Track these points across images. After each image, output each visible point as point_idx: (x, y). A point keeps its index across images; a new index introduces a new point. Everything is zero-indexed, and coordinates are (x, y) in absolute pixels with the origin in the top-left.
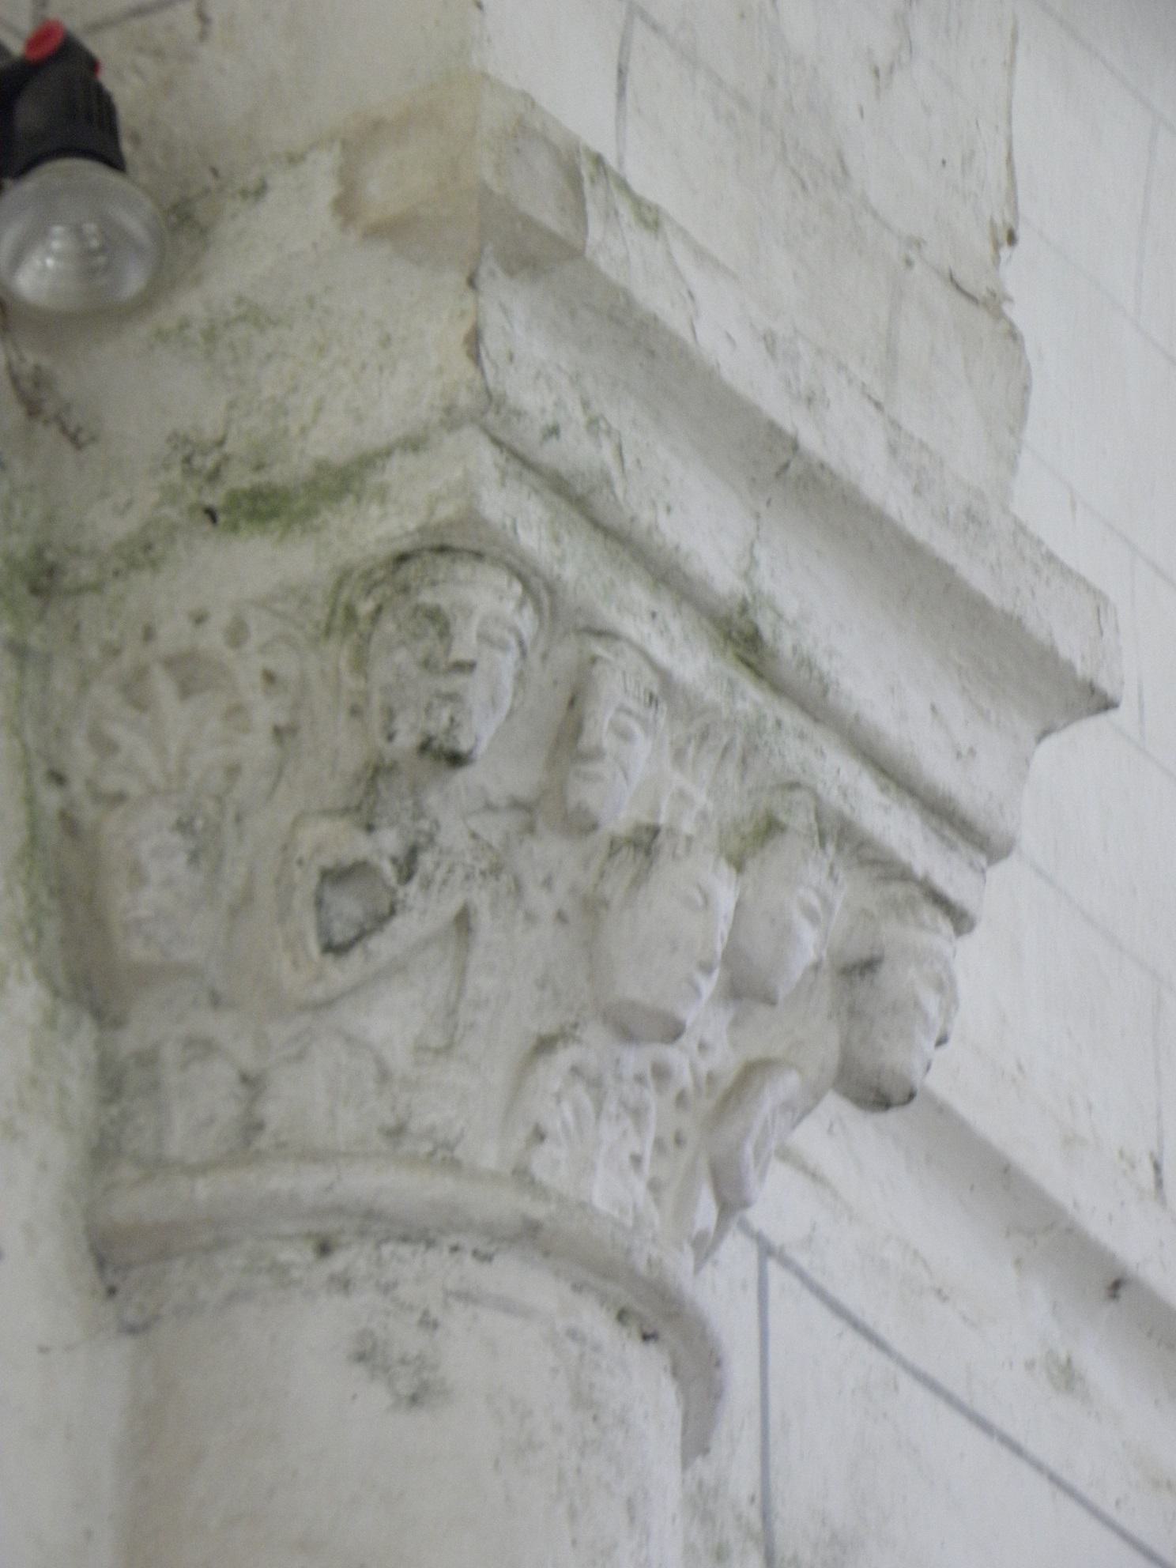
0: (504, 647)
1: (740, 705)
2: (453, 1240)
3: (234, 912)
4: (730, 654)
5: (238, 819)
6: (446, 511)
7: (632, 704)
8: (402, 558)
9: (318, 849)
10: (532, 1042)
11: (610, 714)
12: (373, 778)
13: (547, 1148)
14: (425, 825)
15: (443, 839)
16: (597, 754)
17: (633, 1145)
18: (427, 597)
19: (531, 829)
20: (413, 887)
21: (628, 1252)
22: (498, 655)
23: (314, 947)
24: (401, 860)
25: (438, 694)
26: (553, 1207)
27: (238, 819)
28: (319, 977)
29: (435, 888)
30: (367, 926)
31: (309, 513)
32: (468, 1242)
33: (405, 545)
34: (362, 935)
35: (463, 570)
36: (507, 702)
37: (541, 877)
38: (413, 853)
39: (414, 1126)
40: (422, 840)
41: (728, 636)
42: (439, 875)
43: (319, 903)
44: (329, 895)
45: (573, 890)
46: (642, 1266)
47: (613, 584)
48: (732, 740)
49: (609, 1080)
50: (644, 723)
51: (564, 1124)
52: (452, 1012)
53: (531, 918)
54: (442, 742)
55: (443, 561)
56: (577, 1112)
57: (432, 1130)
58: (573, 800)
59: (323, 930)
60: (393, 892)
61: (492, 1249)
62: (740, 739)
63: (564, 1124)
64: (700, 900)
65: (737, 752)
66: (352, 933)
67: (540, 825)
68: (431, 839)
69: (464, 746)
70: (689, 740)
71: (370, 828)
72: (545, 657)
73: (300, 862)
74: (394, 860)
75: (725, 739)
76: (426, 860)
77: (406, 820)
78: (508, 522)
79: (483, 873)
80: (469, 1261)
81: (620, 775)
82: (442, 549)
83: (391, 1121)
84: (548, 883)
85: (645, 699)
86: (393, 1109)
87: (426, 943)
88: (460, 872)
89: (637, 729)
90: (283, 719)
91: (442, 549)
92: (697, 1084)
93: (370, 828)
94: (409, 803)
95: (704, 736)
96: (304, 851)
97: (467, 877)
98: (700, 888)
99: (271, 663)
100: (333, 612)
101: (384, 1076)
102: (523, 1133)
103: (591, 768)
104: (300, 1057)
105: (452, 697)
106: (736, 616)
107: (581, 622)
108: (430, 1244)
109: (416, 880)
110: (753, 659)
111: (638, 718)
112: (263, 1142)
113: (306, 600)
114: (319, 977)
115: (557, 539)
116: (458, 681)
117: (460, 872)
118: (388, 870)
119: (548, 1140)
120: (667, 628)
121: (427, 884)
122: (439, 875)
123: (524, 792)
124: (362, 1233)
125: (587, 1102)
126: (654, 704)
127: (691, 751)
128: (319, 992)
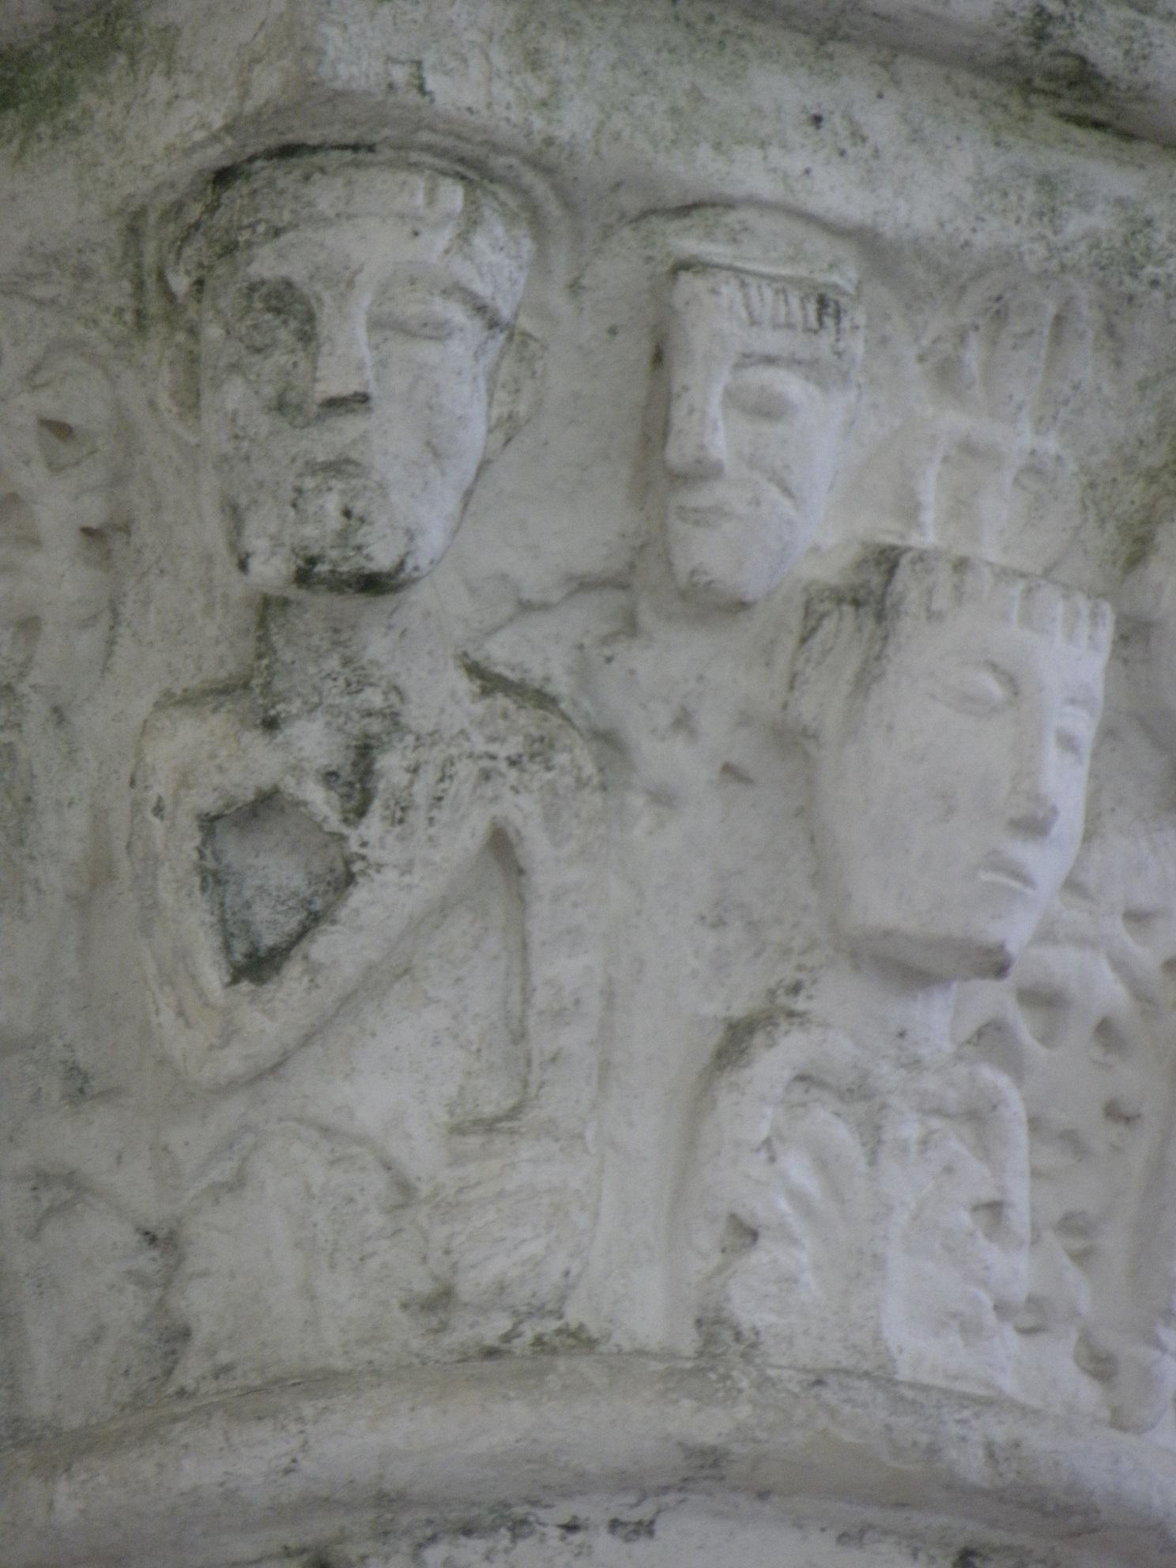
0: (439, 331)
1: (1076, 224)
2: (564, 1511)
3: (82, 904)
4: (1042, 116)
5: (59, 715)
6: (268, 83)
7: (773, 341)
8: (223, 177)
9: (185, 781)
10: (715, 1037)
11: (724, 377)
12: (262, 623)
13: (760, 1257)
14: (374, 698)
15: (416, 716)
16: (703, 472)
17: (977, 1179)
18: (265, 264)
19: (630, 627)
20: (373, 826)
21: (932, 1451)
22: (429, 352)
23: (212, 975)
24: (346, 773)
25: (314, 468)
26: (744, 1411)
27: (59, 715)
28: (229, 1034)
29: (417, 818)
30: (318, 905)
31: (61, 93)
32: (591, 1509)
33: (214, 156)
34: (313, 921)
35: (325, 195)
36: (474, 437)
37: (664, 718)
38: (365, 751)
39: (468, 1286)
40: (375, 726)
41: (1027, 87)
42: (422, 791)
43: (213, 879)
44: (233, 850)
45: (745, 719)
46: (972, 1466)
47: (696, 95)
48: (1069, 302)
49: (887, 1074)
50: (809, 367)
51: (797, 1197)
52: (519, 1036)
53: (663, 798)
54: (339, 560)
55: (286, 176)
56: (823, 1164)
57: (501, 1288)
58: (682, 567)
59: (227, 930)
60: (342, 838)
61: (645, 1512)
62: (1085, 293)
63: (797, 1197)
64: (996, 689)
65: (1088, 315)
66: (292, 923)
67: (646, 619)
68: (393, 718)
69: (382, 559)
70: (962, 338)
71: (271, 725)
72: (575, 288)
73: (158, 810)
74: (330, 777)
75: (1052, 309)
76: (391, 764)
77: (334, 694)
78: (400, 74)
79: (513, 762)
80: (605, 1543)
81: (773, 492)
82: (288, 151)
83: (424, 1287)
84: (683, 722)
85: (805, 317)
86: (424, 1259)
87: (442, 909)
88: (465, 770)
89: (792, 386)
90: (94, 511)
91: (288, 151)
92: (1141, 995)
93: (271, 725)
94: (333, 663)
95: (999, 312)
96: (160, 787)
97: (486, 776)
98: (994, 667)
99: (49, 404)
100: (139, 286)
101: (404, 1191)
102: (707, 1239)
103: (702, 497)
104: (237, 1184)
105: (338, 467)
106: (1026, 53)
107: (631, 202)
108: (519, 1528)
109: (376, 807)
110: (1099, 112)
111: (793, 362)
112: (192, 1369)
113: (84, 273)
114: (229, 1034)
115: (534, 61)
116: (349, 428)
117: (465, 770)
118: (320, 800)
119: (763, 1241)
120: (858, 136)
121: (400, 813)
122: (422, 791)
123: (592, 561)
124: (383, 1533)
125: (842, 1136)
126: (829, 322)
127: (973, 356)
128: (233, 1061)
